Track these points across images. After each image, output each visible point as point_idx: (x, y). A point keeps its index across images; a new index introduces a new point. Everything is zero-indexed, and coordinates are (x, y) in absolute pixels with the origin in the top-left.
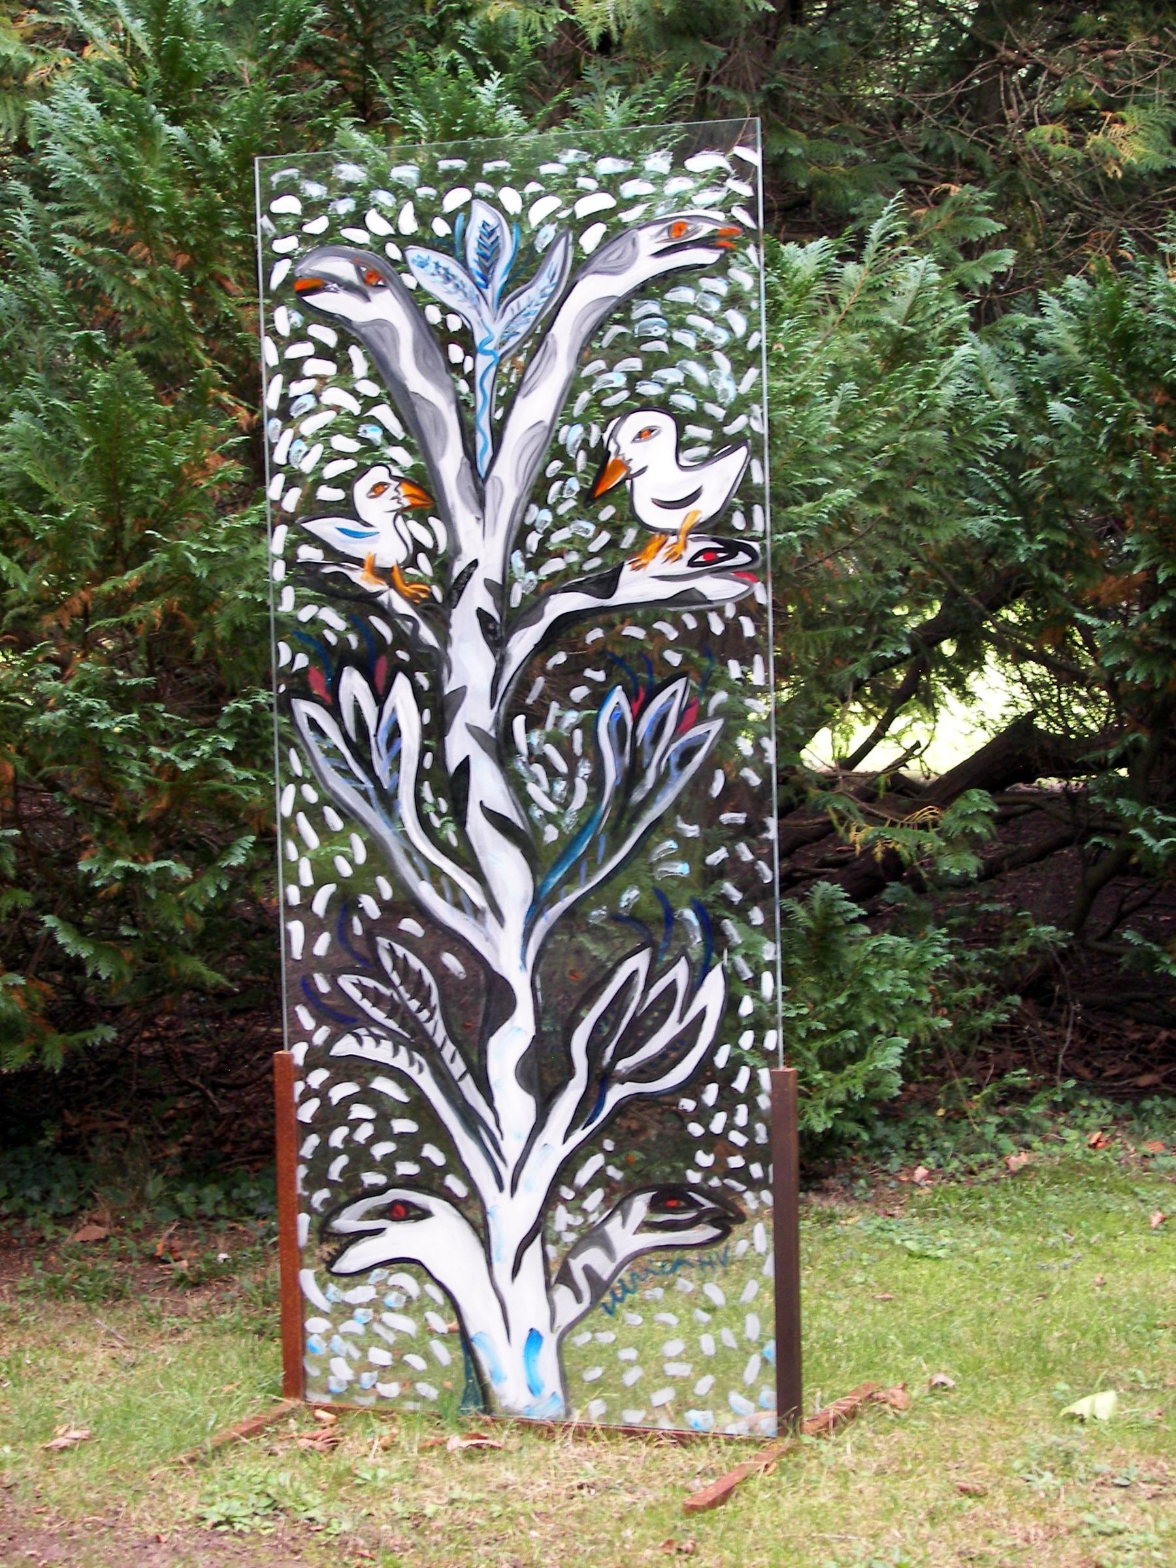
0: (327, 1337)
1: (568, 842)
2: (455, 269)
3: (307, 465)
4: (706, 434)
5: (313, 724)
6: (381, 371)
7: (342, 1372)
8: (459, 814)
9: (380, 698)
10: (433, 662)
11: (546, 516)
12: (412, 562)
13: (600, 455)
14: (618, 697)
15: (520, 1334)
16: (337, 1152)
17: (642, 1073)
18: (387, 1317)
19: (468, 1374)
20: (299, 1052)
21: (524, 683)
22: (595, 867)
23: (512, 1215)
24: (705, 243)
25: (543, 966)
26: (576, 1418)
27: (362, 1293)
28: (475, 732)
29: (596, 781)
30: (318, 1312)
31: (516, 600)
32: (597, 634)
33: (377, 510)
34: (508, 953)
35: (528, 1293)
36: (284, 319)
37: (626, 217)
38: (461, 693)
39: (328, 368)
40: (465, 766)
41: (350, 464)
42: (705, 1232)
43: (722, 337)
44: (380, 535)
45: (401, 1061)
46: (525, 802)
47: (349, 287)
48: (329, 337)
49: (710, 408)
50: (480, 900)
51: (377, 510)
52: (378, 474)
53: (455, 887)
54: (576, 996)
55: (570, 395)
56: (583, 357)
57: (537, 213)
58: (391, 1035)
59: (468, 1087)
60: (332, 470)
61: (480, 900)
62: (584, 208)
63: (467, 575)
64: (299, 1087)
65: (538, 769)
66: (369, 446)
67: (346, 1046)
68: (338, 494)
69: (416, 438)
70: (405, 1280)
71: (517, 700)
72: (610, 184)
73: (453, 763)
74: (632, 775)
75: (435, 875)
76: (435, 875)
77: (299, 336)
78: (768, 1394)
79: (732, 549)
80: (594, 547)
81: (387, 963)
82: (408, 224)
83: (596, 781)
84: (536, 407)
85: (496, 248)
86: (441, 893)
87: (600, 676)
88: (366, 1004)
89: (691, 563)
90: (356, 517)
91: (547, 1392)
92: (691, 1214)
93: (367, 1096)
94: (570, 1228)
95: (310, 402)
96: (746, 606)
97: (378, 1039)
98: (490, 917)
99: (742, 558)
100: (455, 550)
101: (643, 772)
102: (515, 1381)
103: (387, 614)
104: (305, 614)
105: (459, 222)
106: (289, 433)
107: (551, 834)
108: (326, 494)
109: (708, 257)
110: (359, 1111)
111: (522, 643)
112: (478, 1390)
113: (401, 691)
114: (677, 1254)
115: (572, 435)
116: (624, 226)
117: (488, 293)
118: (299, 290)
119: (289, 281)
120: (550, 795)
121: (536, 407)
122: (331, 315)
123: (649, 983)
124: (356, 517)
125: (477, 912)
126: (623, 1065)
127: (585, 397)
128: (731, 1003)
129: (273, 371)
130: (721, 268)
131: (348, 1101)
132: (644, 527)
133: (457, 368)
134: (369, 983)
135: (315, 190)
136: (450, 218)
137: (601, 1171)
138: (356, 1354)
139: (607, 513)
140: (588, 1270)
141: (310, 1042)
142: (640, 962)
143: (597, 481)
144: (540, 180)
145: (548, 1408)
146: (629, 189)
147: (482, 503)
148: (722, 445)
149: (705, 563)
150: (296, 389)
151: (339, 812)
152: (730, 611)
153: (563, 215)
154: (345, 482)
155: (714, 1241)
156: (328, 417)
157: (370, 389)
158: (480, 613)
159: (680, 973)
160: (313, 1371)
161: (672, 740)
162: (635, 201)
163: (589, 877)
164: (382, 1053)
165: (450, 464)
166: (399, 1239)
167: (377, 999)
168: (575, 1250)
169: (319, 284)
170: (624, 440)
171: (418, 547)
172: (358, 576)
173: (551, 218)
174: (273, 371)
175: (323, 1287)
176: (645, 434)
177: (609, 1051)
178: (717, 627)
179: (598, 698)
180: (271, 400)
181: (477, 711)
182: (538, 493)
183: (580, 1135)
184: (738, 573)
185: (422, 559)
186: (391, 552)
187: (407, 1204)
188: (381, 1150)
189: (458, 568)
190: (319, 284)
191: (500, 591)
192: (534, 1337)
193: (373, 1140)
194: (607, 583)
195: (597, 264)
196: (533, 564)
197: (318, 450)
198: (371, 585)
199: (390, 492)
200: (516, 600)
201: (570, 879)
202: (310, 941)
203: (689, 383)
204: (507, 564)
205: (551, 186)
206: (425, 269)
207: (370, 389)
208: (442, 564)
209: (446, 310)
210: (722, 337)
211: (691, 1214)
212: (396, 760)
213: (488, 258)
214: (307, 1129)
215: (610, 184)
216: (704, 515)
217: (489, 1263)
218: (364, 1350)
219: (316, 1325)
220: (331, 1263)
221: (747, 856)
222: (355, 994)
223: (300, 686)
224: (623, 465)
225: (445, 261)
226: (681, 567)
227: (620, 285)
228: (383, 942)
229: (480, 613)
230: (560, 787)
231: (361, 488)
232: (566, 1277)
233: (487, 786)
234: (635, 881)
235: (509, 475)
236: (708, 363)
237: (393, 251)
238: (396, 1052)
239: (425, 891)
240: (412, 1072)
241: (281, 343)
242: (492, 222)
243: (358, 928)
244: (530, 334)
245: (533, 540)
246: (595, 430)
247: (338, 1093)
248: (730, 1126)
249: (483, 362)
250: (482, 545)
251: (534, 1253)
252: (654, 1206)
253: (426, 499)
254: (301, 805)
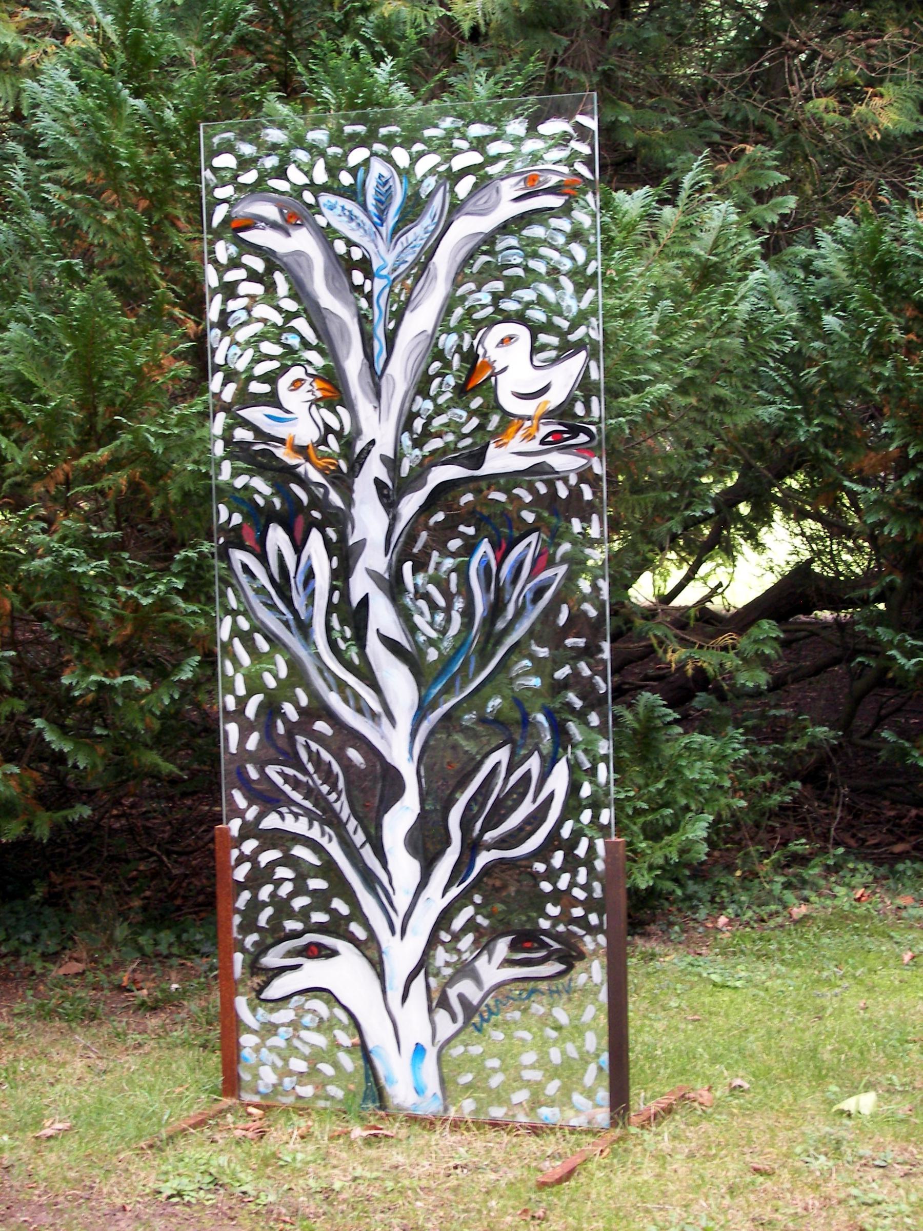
0: (257, 1049)
1: (446, 661)
2: (357, 211)
3: (241, 365)
4: (554, 340)
5: (246, 568)
6: (299, 291)
7: (268, 1077)
8: (360, 639)
9: (298, 548)
10: (340, 520)
11: (429, 405)
12: (324, 441)
13: (471, 358)
14: (485, 547)
15: (408, 1048)
16: (264, 905)
17: (504, 843)
18: (303, 1034)
19: (367, 1079)
20: (235, 826)
21: (411, 536)
22: (467, 681)
23: (402, 954)
24: (554, 191)
25: (426, 758)
26: (452, 1113)
27: (284, 1015)
28: (373, 575)
29: (468, 613)
30: (250, 1030)
31: (405, 471)
32: (468, 497)
33: (296, 400)
34: (399, 748)
35: (414, 1015)
36: (223, 251)
37: (492, 170)
38: (362, 544)
39: (257, 289)
40: (365, 601)
41: (275, 365)
42: (553, 967)
43: (566, 265)
44: (298, 420)
45: (315, 833)
46: (412, 629)
47: (274, 225)
48: (258, 265)
49: (558, 321)
50: (376, 707)
51: (296, 400)
52: (297, 372)
53: (357, 696)
54: (452, 782)
56: (457, 280)
57: (422, 167)
58: (307, 812)
59: (368, 854)
60: (261, 369)
61: (376, 707)
62: (458, 163)
63: (366, 451)
64: (235, 853)
65: (422, 604)
66: (290, 350)
67: (271, 821)
68: (265, 388)
69: (326, 344)
70: (318, 1005)
71: (406, 550)
72: (479, 145)
73: (355, 599)
74: (496, 608)
75: (341, 687)
76: (341, 687)
77: (235, 264)
78: (603, 1095)
79: (575, 431)
80: (466, 430)
81: (304, 756)
82: (320, 176)
83: (468, 613)
84: (421, 319)
85: (389, 195)
86: (346, 701)
87: (471, 531)
88: (287, 788)
89: (542, 442)
90: (279, 406)
91: (429, 1093)
92: (543, 953)
93: (288, 860)
94: (447, 964)
95: (243, 315)
96: (586, 475)
97: (296, 816)
98: (385, 720)
99: (583, 438)
100: (357, 432)
101: (505, 606)
102: (404, 1084)
103: (303, 482)
104: (239, 482)
105: (361, 174)
106: (227, 340)
107: (432, 655)
108: (256, 387)
109: (555, 201)
110: (282, 872)
111: (410, 505)
112: (375, 1091)
113: (315, 543)
114: (532, 984)
115: (449, 342)
116: (490, 177)
117: (383, 230)
118: (235, 228)
119: (227, 221)
120: (431, 624)
121: (421, 319)
122: (259, 248)
123: (510, 772)
124: (279, 406)
125: (374, 716)
126: (489, 836)
127: (459, 311)
128: (574, 788)
130: (566, 211)
131: (273, 864)
132: (506, 414)
133: (359, 289)
134: (290, 771)
135: (247, 149)
136: (353, 171)
137: (472, 920)
138: (280, 1063)
139: (476, 403)
140: (461, 997)
141: (243, 818)
142: (502, 755)
143: (469, 378)
144: (424, 142)
145: (430, 1106)
146: (494, 148)
147: (378, 395)
148: (567, 349)
149: (554, 442)
150: (232, 305)
151: (266, 638)
152: (573, 480)
153: (442, 168)
154: (271, 378)
155: (560, 974)
156: (257, 327)
157: (291, 305)
158: (377, 481)
159: (534, 764)
160: (246, 1076)
161: (528, 581)
162: (498, 157)
163: (462, 688)
164: (300, 826)
165: (353, 364)
166: (313, 973)
167: (296, 784)
168: (451, 981)
169: (251, 223)
170: (490, 345)
171: (328, 429)
172: (281, 453)
173: (432, 171)
174: (215, 292)
175: (253, 1010)
176: (506, 341)
177: (478, 825)
178: (563, 492)
179: (469, 548)
180: (213, 314)
181: (375, 558)
182: (422, 387)
183: (455, 891)
184: (579, 449)
185: (331, 439)
186: (307, 434)
187: (319, 945)
188: (299, 903)
189: (359, 446)
190: (251, 223)
191: (393, 464)
192: (419, 1050)
193: (292, 895)
194: (476, 458)
195: (469, 207)
196: (418, 443)
197: (249, 353)
198: (291, 460)
199: (306, 387)
200: (405, 471)
201: (448, 690)
202: (243, 739)
203: (541, 301)
204: (398, 442)
205: (433, 146)
206: (334, 212)
207: (291, 305)
208: (347, 443)
209: (350, 243)
210: (567, 265)
211: (543, 953)
212: (311, 597)
213: (383, 203)
214: (241, 886)
215: (479, 145)
216: (553, 405)
217: (384, 991)
218: (286, 1060)
219: (248, 1041)
220: (259, 992)
221: (586, 672)
222: (279, 781)
223: (236, 539)
224: (489, 365)
225: (350, 205)
226: (535, 445)
227: (486, 224)
228: (300, 739)
229: (377, 481)
230: (440, 618)
231: (284, 383)
232: (444, 1003)
233: (383, 617)
234: (498, 692)
235: (400, 373)
236: (555, 285)
237: (308, 197)
238: (311, 826)
239: (334, 700)
240: (324, 841)
241: (221, 269)
242: (386, 174)
243: (281, 728)
244: (416, 262)
245: (418, 424)
246: (467, 337)
247: (265, 858)
248: (573, 884)
249: (379, 284)
250: (378, 428)
251: (419, 983)
252: (513, 947)
253: (334, 392)
254: (236, 632)
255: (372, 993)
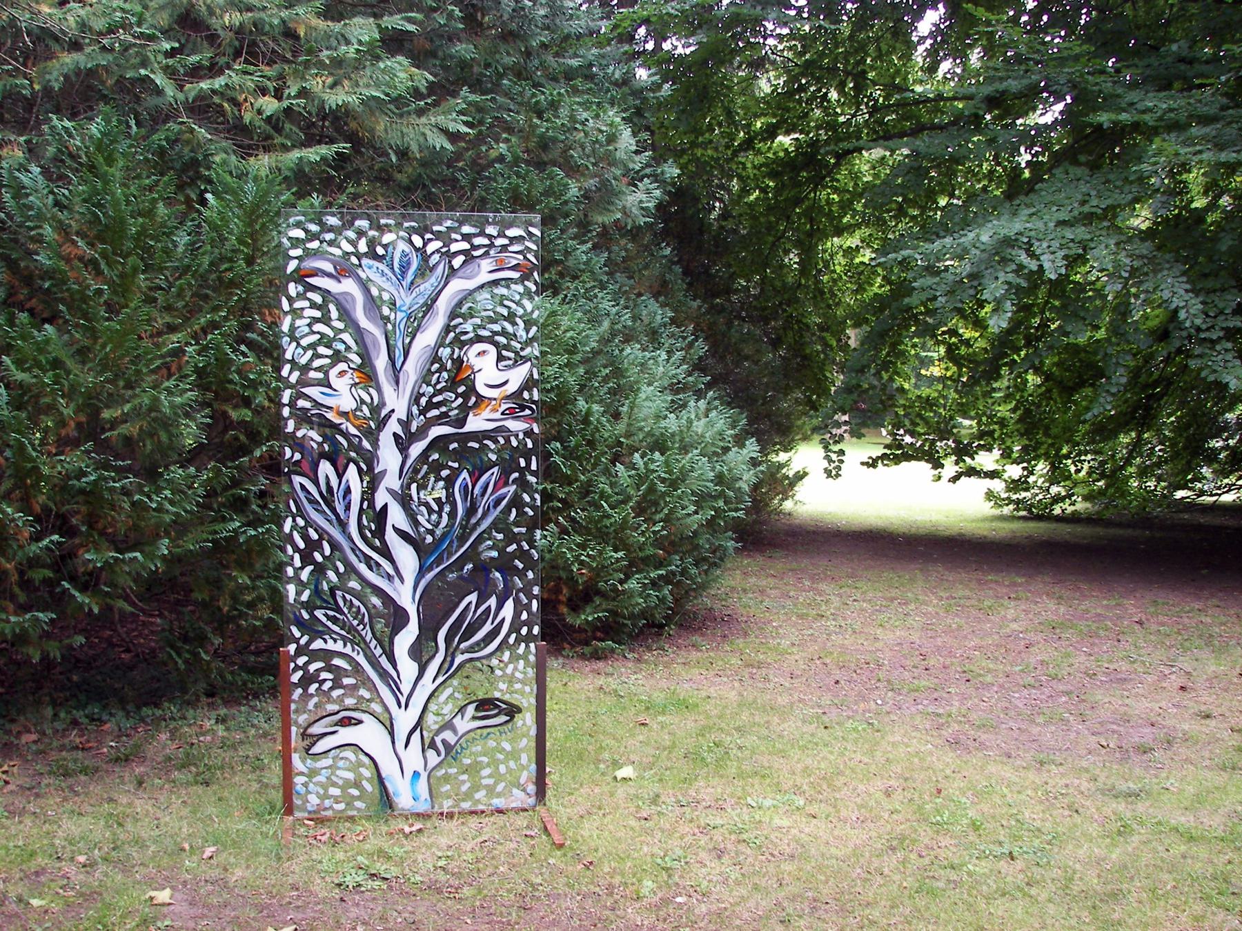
0: (305, 785)
1: (438, 543)
2: (387, 271)
3: (303, 361)
4: (512, 355)
5: (302, 486)
6: (345, 315)
7: (314, 800)
8: (380, 532)
9: (340, 476)
10: (370, 459)
11: (431, 389)
12: (358, 409)
13: (458, 363)
14: (465, 474)
15: (409, 773)
16: (312, 695)
17: (471, 650)
18: (338, 772)
19: (382, 796)
20: (292, 648)
21: (416, 471)
22: (450, 555)
23: (405, 720)
24: (513, 268)
25: (426, 601)
26: (436, 809)
27: (326, 762)
28: (391, 491)
29: (453, 514)
30: (302, 774)
31: (413, 429)
32: (455, 445)
33: (341, 384)
34: (406, 597)
35: (413, 757)
36: (293, 289)
37: (476, 253)
38: (384, 472)
39: (318, 314)
40: (385, 507)
41: (328, 361)
42: (504, 718)
43: (520, 311)
44: (343, 396)
45: (348, 650)
46: (416, 523)
47: (329, 275)
48: (318, 299)
49: (513, 343)
50: (391, 572)
51: (341, 384)
52: (342, 366)
53: (378, 565)
54: (441, 614)
55: (447, 329)
56: (453, 315)
57: (431, 247)
58: (343, 638)
59: (384, 661)
60: (317, 363)
61: (391, 572)
62: (455, 247)
63: (389, 416)
64: (292, 665)
65: (423, 509)
66: (337, 352)
67: (318, 644)
68: (320, 375)
69: (365, 355)
70: (348, 754)
71: (411, 475)
72: (467, 237)
73: (378, 506)
74: (471, 511)
75: (368, 560)
76: (368, 560)
77: (301, 296)
78: (532, 788)
79: (523, 408)
80: (454, 405)
81: (341, 603)
82: (363, 247)
83: (453, 514)
84: (428, 337)
85: (409, 263)
86: (370, 568)
87: (456, 465)
88: (329, 624)
89: (503, 414)
90: (330, 387)
91: (422, 799)
92: (496, 711)
93: (329, 668)
94: (436, 723)
95: (307, 330)
96: (529, 433)
97: (335, 641)
98: (396, 579)
99: (528, 412)
100: (382, 404)
101: (476, 511)
102: (404, 796)
103: (346, 435)
104: (299, 434)
105: (390, 249)
106: (294, 344)
107: (429, 539)
108: (312, 374)
109: (515, 275)
110: (324, 675)
111: (416, 449)
112: (386, 799)
113: (352, 472)
114: (489, 730)
115: (445, 352)
116: (473, 257)
117: (404, 283)
118: (301, 277)
119: (297, 270)
120: (428, 521)
121: (428, 337)
122: (320, 289)
123: (477, 607)
124: (330, 387)
125: (389, 577)
126: (462, 646)
127: (452, 334)
128: (517, 614)
129: (289, 361)
130: (522, 280)
131: (318, 671)
132: (479, 396)
133: (387, 319)
134: (331, 613)
135: (314, 228)
136: (385, 247)
137: (452, 694)
138: (322, 792)
139: (461, 389)
140: (444, 741)
141: (298, 643)
142: (473, 598)
143: (457, 375)
144: (432, 233)
145: (423, 807)
146: (478, 241)
147: (397, 383)
148: (519, 360)
149: (509, 414)
150: (298, 323)
151: (316, 530)
152: (521, 436)
153: (444, 250)
154: (324, 370)
155: (507, 722)
156: (314, 338)
157: (340, 325)
158: (395, 434)
159: (493, 602)
160: (297, 801)
161: (492, 494)
162: (479, 247)
163: (448, 559)
164: (339, 647)
165: (381, 362)
166: (346, 735)
167: (334, 620)
168: (438, 732)
169: (316, 273)
170: (471, 354)
171: (363, 402)
172: (330, 416)
173: (438, 251)
174: (286, 313)
175: (303, 762)
176: (482, 353)
177: (457, 639)
178: (514, 443)
179: (455, 474)
180: (285, 328)
181: (392, 481)
182: (425, 379)
183: (440, 679)
184: (525, 419)
185: (365, 408)
186: (348, 404)
187: (350, 718)
188: (336, 693)
189: (384, 413)
190: (316, 273)
191: (405, 424)
192: (416, 774)
193: (331, 689)
194: (461, 422)
195: (460, 273)
196: (423, 412)
197: (310, 353)
198: (337, 420)
199: (349, 375)
200: (413, 429)
201: (439, 561)
202: (299, 593)
203: (504, 333)
204: (409, 413)
205: (438, 236)
206: (370, 269)
207: (340, 325)
208: (375, 410)
209: (381, 290)
210: (520, 311)
211: (496, 711)
212: (348, 508)
213: (404, 268)
214: (296, 685)
215: (467, 237)
216: (509, 393)
217: (393, 742)
218: (326, 790)
219: (299, 780)
220: (307, 750)
221: (526, 547)
222: (324, 619)
223: (297, 468)
224: (471, 367)
225: (382, 266)
226: (498, 415)
227: (471, 284)
228: (339, 593)
229: (395, 434)
230: (434, 517)
231: (333, 373)
232: (433, 745)
233: (397, 516)
234: (471, 560)
235: (412, 369)
236: (514, 324)
237: (354, 260)
238: (345, 645)
239: (362, 568)
240: (354, 655)
241: (291, 300)
242: (407, 250)
243: (325, 587)
244: (425, 304)
245: (423, 401)
246: (457, 350)
247: (312, 668)
248: (516, 669)
249: (400, 315)
250: (397, 402)
251: (416, 737)
252: (477, 709)
253: (367, 375)
254: (295, 527)
255: (382, 731)
